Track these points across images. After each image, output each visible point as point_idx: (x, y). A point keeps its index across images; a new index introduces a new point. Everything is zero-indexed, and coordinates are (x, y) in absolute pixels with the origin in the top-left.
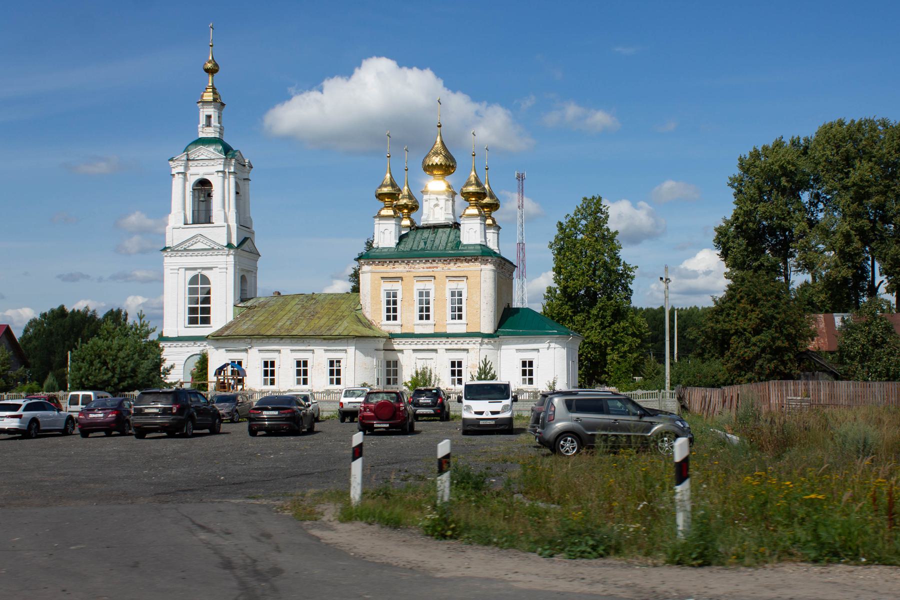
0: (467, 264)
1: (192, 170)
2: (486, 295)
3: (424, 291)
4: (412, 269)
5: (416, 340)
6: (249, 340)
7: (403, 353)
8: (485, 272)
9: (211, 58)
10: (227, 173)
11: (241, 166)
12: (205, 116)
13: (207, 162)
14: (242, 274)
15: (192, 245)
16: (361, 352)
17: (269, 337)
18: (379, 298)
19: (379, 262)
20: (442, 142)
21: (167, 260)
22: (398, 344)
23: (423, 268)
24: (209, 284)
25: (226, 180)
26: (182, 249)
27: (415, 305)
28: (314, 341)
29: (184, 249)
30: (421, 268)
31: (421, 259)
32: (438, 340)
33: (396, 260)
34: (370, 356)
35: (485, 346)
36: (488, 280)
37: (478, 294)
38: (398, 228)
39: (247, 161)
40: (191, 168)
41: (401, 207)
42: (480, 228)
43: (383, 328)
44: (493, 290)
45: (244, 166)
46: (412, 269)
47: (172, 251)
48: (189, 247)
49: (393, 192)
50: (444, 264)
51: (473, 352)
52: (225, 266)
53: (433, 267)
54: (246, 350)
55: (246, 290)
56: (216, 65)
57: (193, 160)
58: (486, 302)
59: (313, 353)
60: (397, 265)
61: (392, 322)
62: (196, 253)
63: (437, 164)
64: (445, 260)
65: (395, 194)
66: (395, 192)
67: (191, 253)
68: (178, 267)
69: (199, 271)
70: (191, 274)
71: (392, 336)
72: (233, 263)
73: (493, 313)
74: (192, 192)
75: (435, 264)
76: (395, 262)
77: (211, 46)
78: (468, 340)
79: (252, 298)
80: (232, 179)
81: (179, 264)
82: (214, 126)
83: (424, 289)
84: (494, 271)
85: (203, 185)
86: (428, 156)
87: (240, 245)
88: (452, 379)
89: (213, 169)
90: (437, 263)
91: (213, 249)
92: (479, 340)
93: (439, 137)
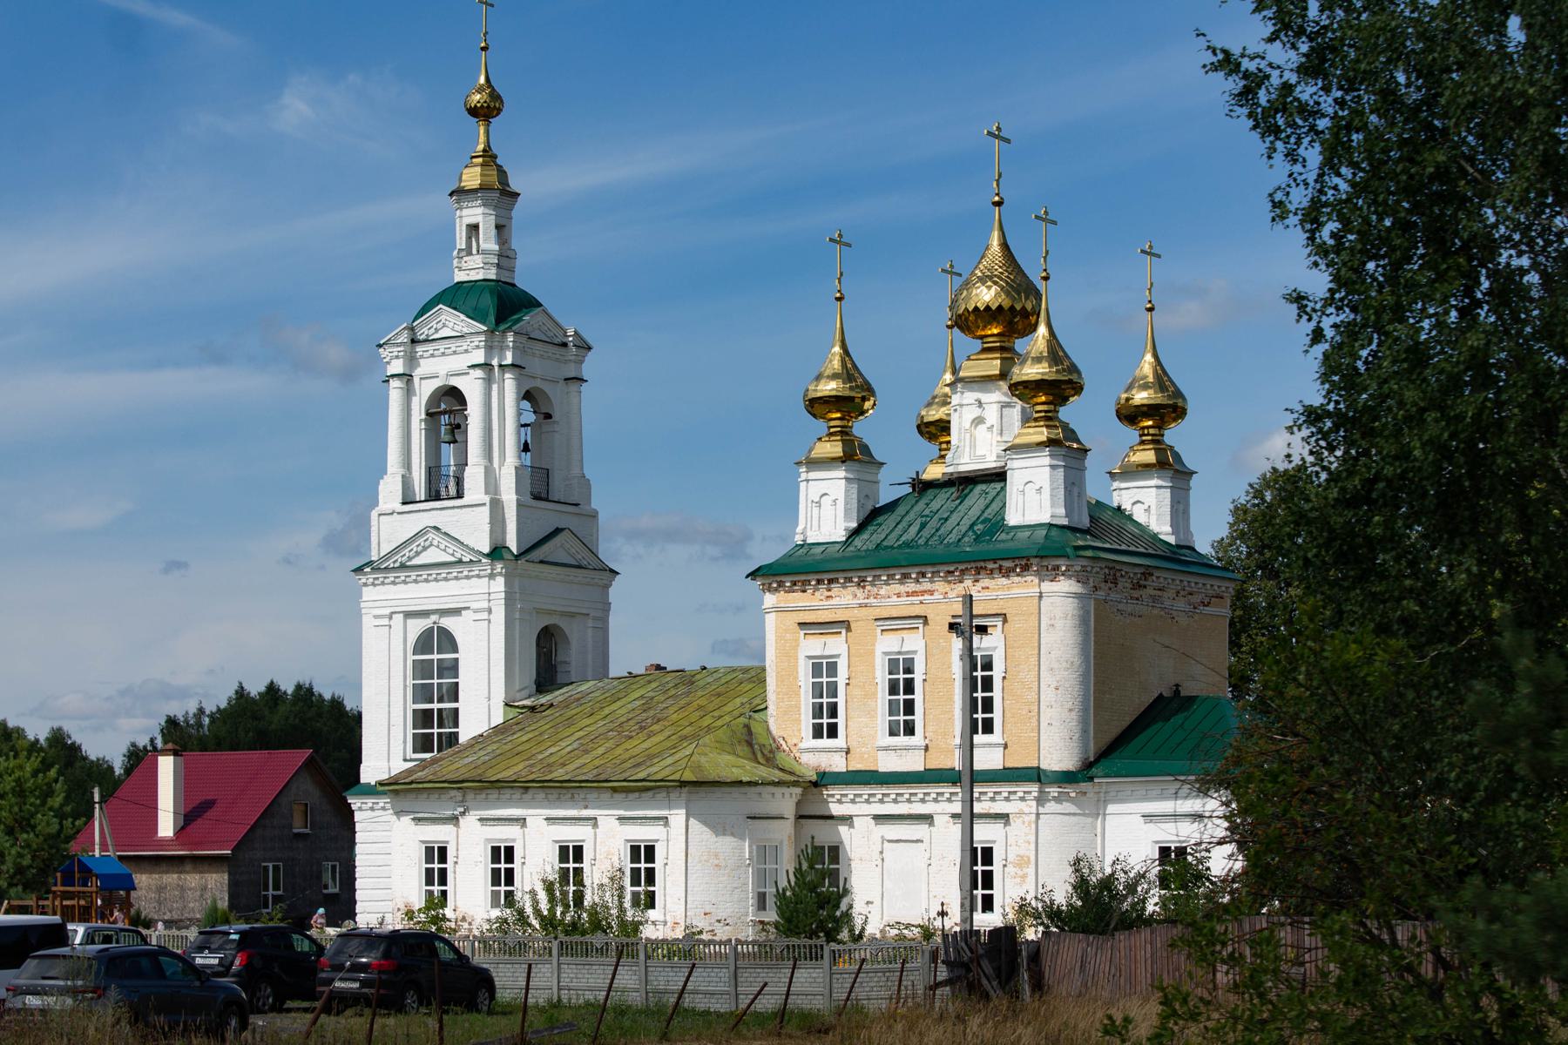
0: (1004, 581)
1: (425, 367)
2: (1056, 666)
3: (901, 657)
4: (872, 600)
5: (879, 791)
7: (851, 826)
8: (1051, 600)
9: (482, 80)
10: (496, 369)
11: (556, 348)
12: (464, 228)
13: (453, 345)
14: (546, 621)
15: (418, 554)
16: (705, 823)
17: (499, 785)
18: (874, 678)
19: (794, 584)
20: (1005, 246)
21: (369, 593)
22: (839, 801)
23: (899, 595)
24: (455, 649)
25: (495, 387)
26: (397, 565)
27: (880, 695)
28: (595, 795)
29: (398, 567)
30: (892, 596)
31: (892, 572)
32: (933, 790)
33: (832, 576)
34: (733, 835)
35: (1051, 806)
36: (1059, 624)
37: (1034, 660)
38: (855, 491)
39: (570, 332)
40: (421, 361)
41: (932, 429)
42: (1052, 482)
43: (806, 758)
44: (1076, 651)
45: (565, 345)
46: (872, 600)
47: (376, 570)
48: (410, 559)
49: (847, 393)
50: (949, 582)
51: (1019, 821)
52: (485, 605)
53: (923, 593)
54: (454, 820)
56: (495, 96)
57: (426, 341)
58: (1055, 684)
59: (595, 825)
60: (836, 589)
61: (825, 742)
62: (424, 573)
63: (988, 308)
64: (949, 572)
65: (851, 399)
66: (853, 394)
67: (413, 575)
68: (387, 611)
69: (434, 618)
70: (417, 627)
71: (824, 780)
72: (503, 595)
73: (1074, 715)
74: (425, 420)
75: (926, 586)
76: (831, 581)
77: (483, 49)
78: (1005, 789)
79: (572, 683)
80: (510, 382)
82: (485, 253)
83: (899, 653)
84: (1077, 596)
85: (449, 402)
86: (967, 285)
87: (523, 554)
89: (462, 362)
90: (932, 582)
91: (460, 562)
92: (1034, 788)
93: (996, 235)
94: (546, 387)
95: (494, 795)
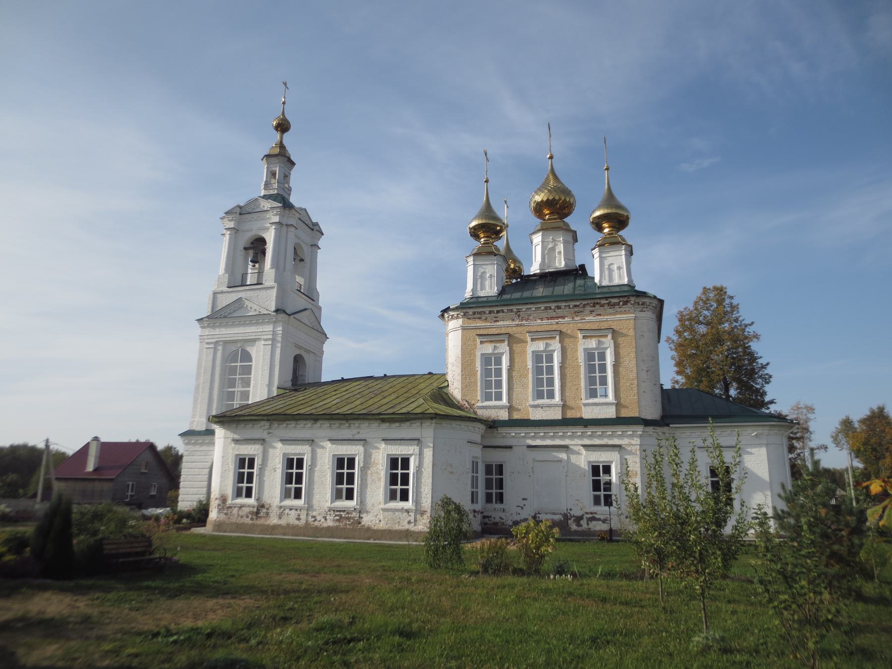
0: (611, 311)
6: (267, 424)
14: (298, 352)
15: (234, 311)
18: (526, 366)
19: (474, 313)
23: (542, 319)
46: (524, 322)
53: (558, 318)
55: (305, 376)
58: (645, 369)
81: (216, 336)
88: (239, 473)
94: (303, 245)
95: (293, 424)
